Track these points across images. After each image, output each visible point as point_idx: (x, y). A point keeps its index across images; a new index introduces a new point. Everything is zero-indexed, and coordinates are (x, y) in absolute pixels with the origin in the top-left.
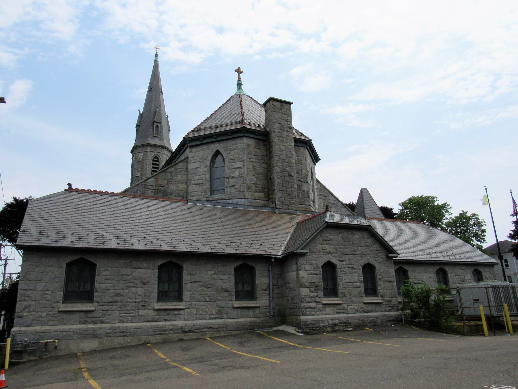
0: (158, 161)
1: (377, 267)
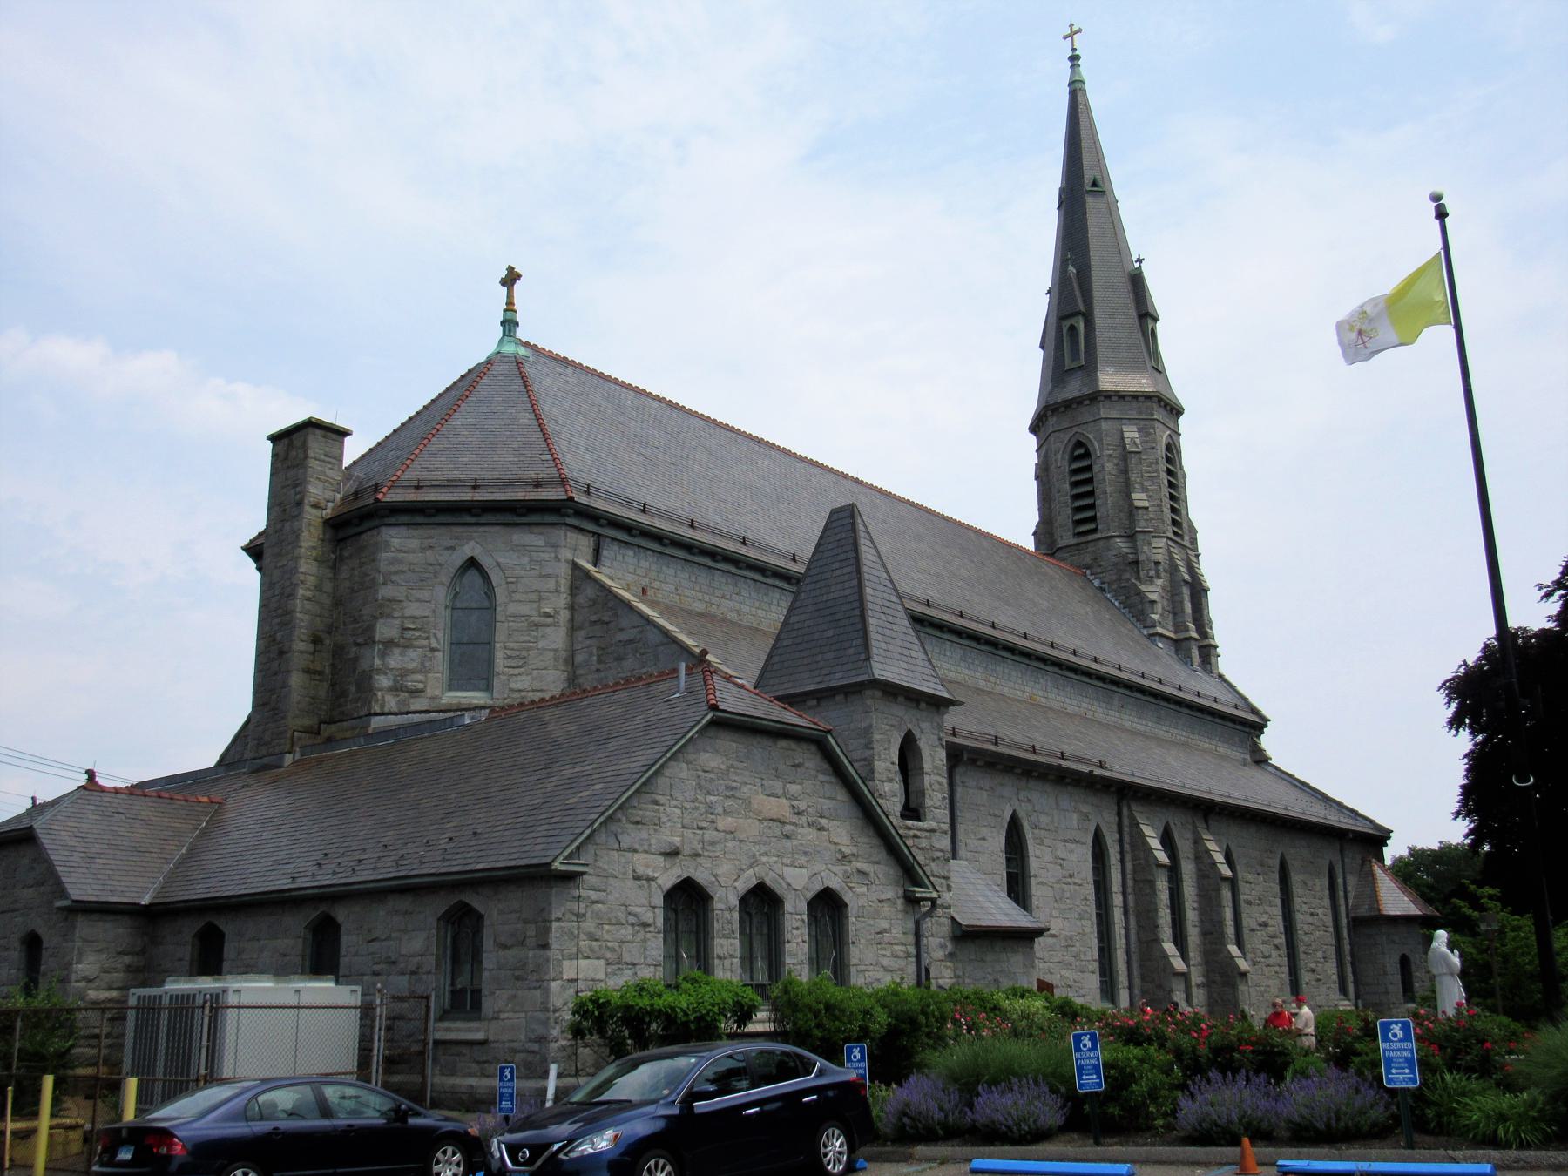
0: (1087, 455)
1: (45, 939)
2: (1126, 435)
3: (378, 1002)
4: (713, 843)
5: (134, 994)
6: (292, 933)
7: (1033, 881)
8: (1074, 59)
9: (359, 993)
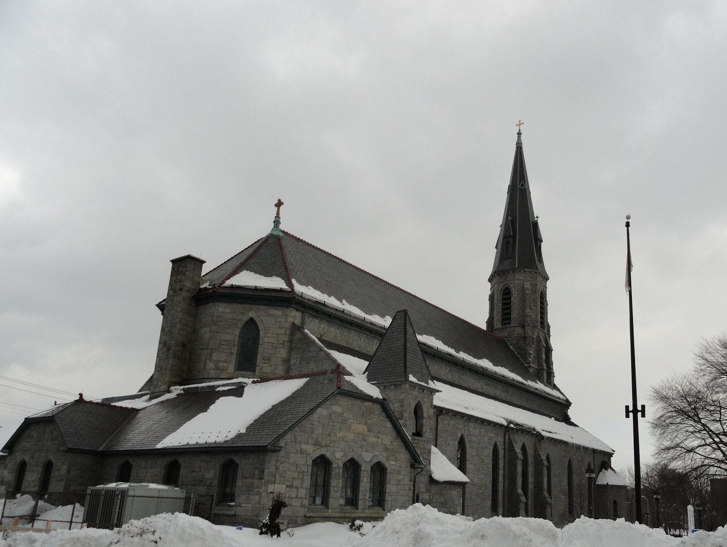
2: (525, 286)
3: (192, 497)
4: (334, 442)
5: (90, 489)
6: (159, 466)
7: (467, 463)
8: (519, 134)
9: (185, 492)
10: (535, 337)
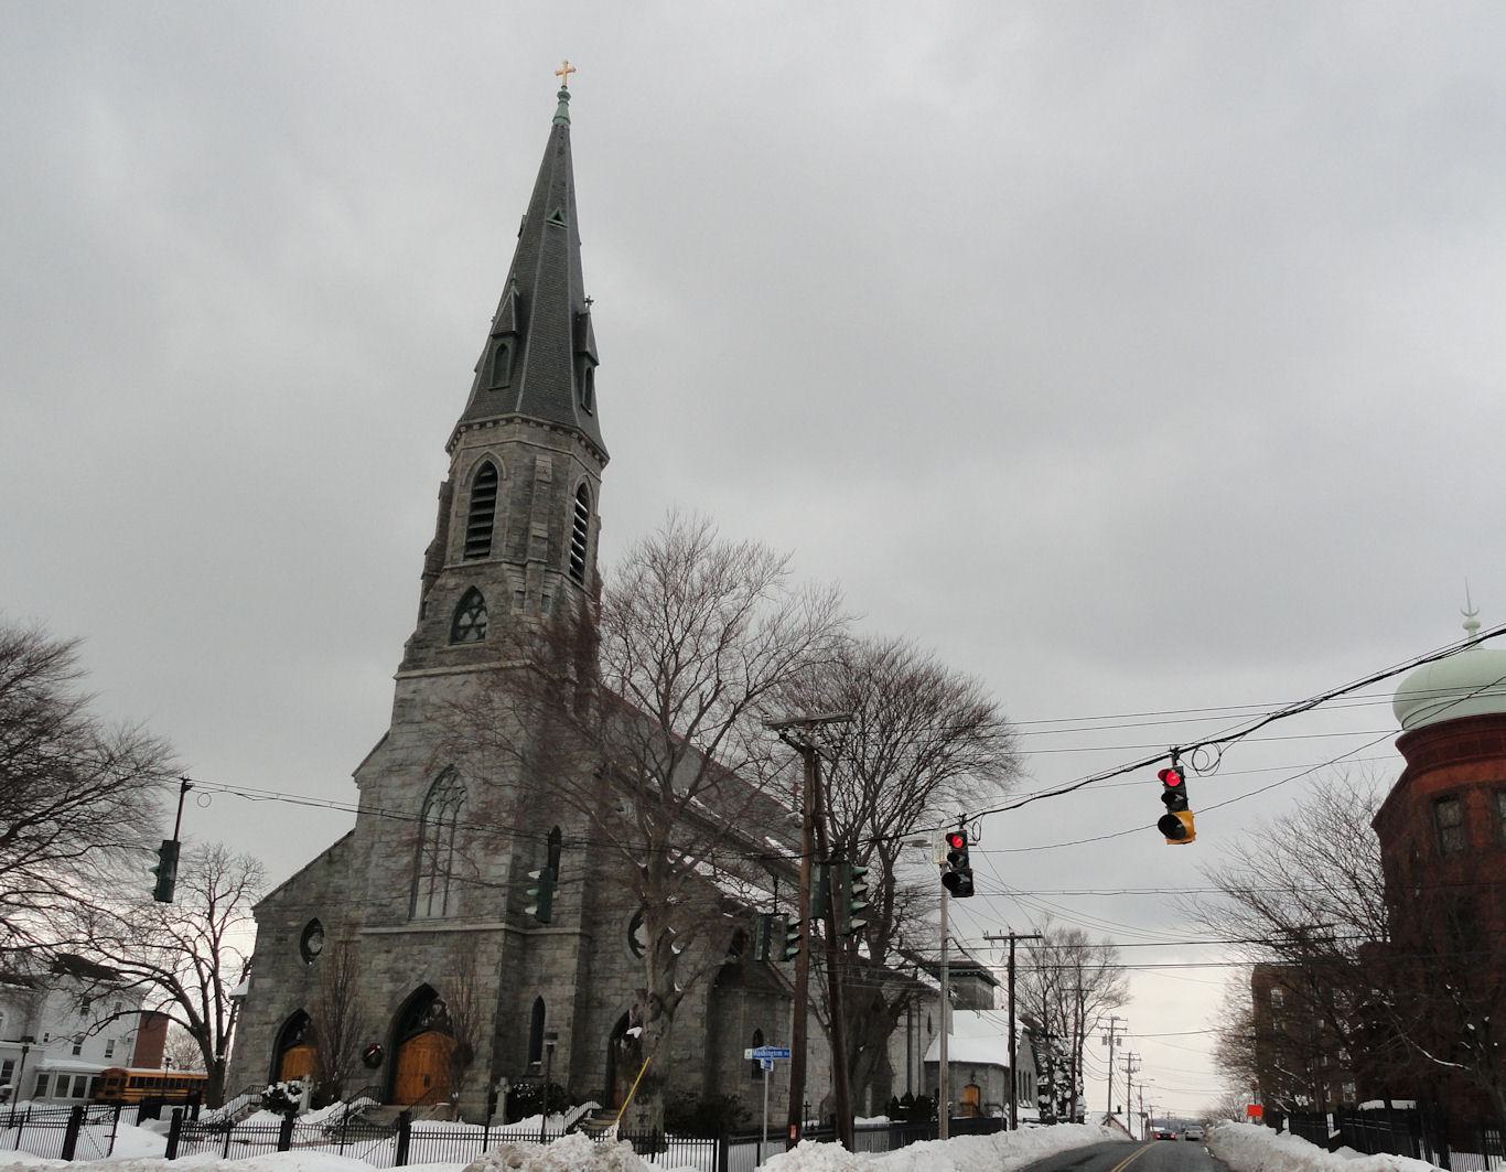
8: (564, 96)
10: (550, 592)
